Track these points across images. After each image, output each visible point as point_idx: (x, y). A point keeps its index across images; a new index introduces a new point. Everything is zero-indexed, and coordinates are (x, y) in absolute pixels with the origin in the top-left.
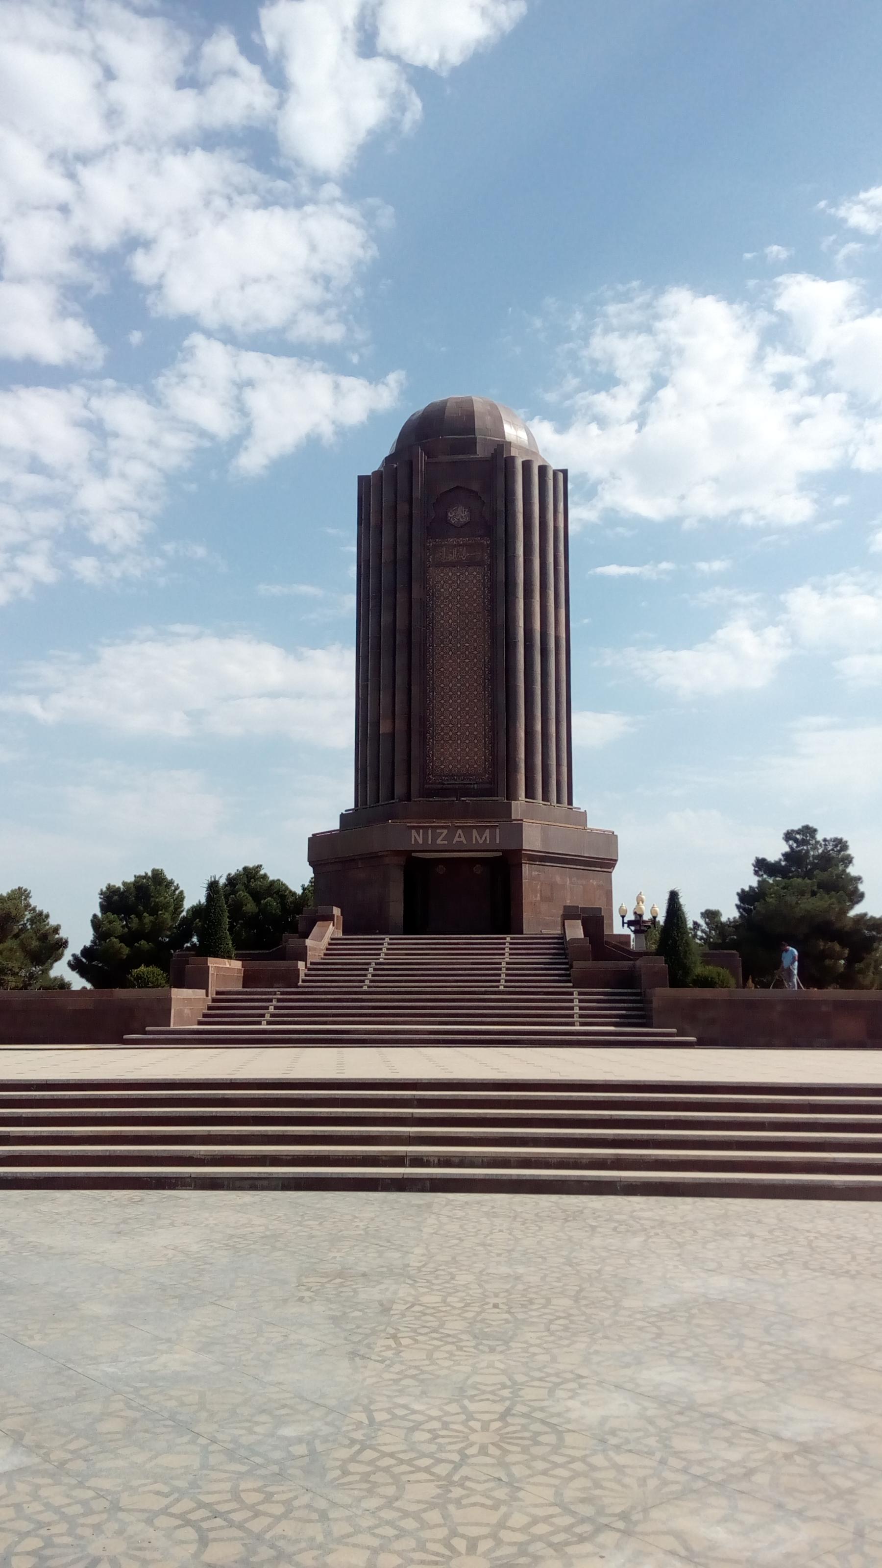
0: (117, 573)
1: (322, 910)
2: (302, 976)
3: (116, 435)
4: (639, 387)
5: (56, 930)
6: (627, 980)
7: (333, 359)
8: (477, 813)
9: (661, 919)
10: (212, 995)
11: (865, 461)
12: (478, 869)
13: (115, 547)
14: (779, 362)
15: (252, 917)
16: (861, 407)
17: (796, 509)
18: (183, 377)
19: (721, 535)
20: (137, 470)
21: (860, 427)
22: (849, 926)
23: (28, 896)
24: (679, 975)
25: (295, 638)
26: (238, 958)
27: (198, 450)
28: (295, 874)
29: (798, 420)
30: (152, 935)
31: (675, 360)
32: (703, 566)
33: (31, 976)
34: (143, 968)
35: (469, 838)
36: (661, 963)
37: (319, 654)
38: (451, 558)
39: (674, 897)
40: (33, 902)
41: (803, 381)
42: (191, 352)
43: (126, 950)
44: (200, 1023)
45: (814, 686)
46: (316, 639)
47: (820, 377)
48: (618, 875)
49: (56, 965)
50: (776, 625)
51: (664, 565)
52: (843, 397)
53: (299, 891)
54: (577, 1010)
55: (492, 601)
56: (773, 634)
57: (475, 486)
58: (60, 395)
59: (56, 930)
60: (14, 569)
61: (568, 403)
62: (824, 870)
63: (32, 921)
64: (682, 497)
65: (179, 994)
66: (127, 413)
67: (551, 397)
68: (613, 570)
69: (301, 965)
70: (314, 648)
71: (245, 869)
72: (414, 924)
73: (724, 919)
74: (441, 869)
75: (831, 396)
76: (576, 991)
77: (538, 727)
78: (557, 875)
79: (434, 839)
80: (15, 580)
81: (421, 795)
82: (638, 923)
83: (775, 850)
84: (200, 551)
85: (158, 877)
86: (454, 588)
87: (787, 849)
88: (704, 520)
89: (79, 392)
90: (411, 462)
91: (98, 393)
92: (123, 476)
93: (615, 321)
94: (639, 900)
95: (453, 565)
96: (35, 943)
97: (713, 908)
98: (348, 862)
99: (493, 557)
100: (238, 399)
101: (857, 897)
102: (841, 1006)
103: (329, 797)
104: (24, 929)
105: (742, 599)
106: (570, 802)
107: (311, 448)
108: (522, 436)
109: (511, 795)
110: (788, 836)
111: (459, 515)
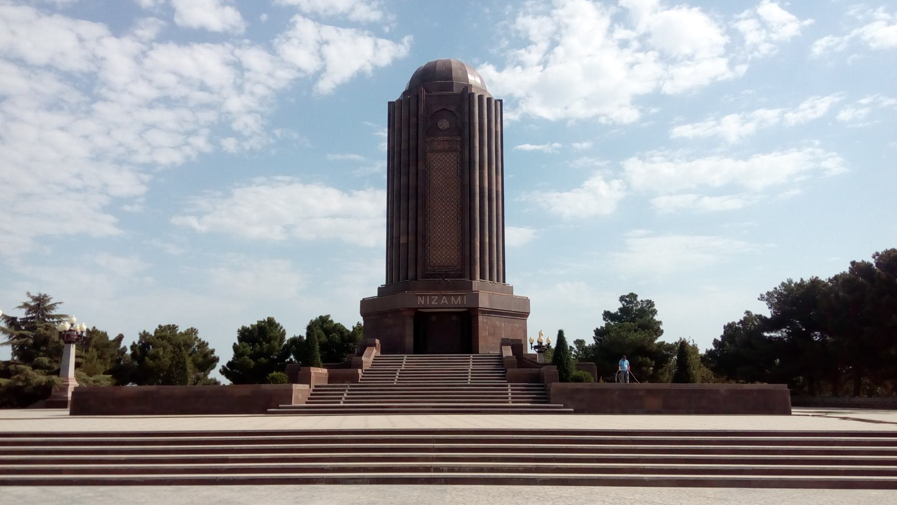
0: (248, 148)
1: (369, 340)
2: (360, 377)
3: (249, 70)
4: (544, 46)
5: (212, 351)
6: (537, 379)
7: (374, 30)
8: (455, 288)
9: (553, 345)
10: (313, 387)
11: (668, 88)
12: (454, 318)
13: (247, 133)
14: (621, 33)
15: (328, 345)
16: (667, 59)
17: (630, 115)
18: (288, 39)
19: (588, 128)
20: (260, 90)
21: (666, 70)
22: (655, 348)
23: (196, 333)
24: (564, 376)
25: (348, 184)
26: (324, 367)
27: (297, 79)
28: (350, 318)
29: (632, 66)
30: (267, 355)
31: (563, 31)
32: (577, 145)
33: (198, 379)
34: (275, 373)
35: (449, 301)
36: (554, 369)
37: (361, 193)
38: (439, 147)
39: (561, 333)
40: (199, 336)
41: (635, 45)
42: (293, 25)
43: (253, 363)
44: (307, 403)
45: (639, 212)
46: (359, 185)
47: (645, 42)
48: (529, 320)
49: (212, 372)
50: (618, 178)
51: (556, 145)
52: (656, 54)
53: (351, 330)
54: (510, 395)
55: (462, 171)
56: (616, 183)
57: (453, 109)
58: (219, 48)
59: (212, 351)
60: (187, 144)
61: (503, 55)
62: (641, 318)
63: (199, 347)
64: (566, 108)
65: (296, 387)
66: (255, 59)
67: (494, 51)
68: (528, 147)
69: (360, 371)
70: (359, 190)
71: (321, 317)
72: (419, 348)
73: (587, 345)
74: (434, 318)
75: (651, 53)
76: (509, 385)
77: (487, 240)
78: (496, 320)
79: (430, 302)
80: (187, 150)
81: (423, 277)
82: (540, 347)
83: (615, 307)
84: (296, 136)
85: (271, 322)
86: (441, 165)
87: (621, 306)
88: (578, 121)
89: (229, 46)
90: (417, 96)
91: (240, 46)
92: (252, 94)
93: (530, 10)
94: (541, 334)
95: (440, 151)
96: (200, 360)
97: (580, 338)
98: (382, 314)
99: (462, 147)
100: (319, 51)
101: (659, 332)
102: (649, 392)
103: (371, 276)
104: (194, 351)
105: (598, 164)
106: (504, 281)
107: (360, 78)
108: (478, 80)
109: (472, 277)
110: (622, 299)
111: (444, 124)
